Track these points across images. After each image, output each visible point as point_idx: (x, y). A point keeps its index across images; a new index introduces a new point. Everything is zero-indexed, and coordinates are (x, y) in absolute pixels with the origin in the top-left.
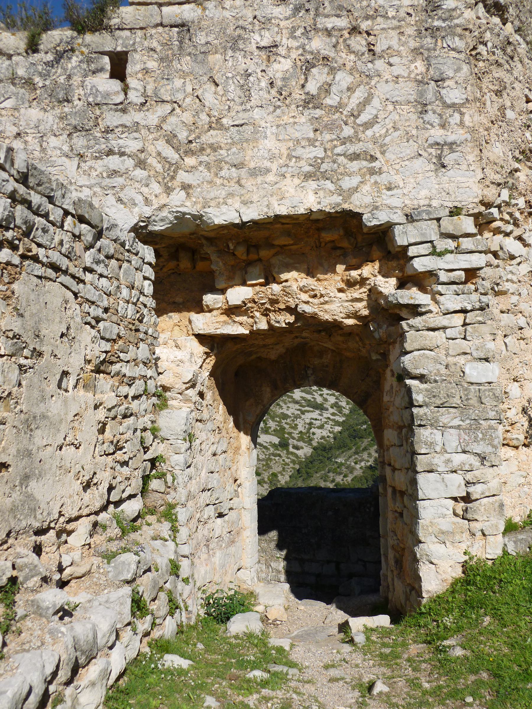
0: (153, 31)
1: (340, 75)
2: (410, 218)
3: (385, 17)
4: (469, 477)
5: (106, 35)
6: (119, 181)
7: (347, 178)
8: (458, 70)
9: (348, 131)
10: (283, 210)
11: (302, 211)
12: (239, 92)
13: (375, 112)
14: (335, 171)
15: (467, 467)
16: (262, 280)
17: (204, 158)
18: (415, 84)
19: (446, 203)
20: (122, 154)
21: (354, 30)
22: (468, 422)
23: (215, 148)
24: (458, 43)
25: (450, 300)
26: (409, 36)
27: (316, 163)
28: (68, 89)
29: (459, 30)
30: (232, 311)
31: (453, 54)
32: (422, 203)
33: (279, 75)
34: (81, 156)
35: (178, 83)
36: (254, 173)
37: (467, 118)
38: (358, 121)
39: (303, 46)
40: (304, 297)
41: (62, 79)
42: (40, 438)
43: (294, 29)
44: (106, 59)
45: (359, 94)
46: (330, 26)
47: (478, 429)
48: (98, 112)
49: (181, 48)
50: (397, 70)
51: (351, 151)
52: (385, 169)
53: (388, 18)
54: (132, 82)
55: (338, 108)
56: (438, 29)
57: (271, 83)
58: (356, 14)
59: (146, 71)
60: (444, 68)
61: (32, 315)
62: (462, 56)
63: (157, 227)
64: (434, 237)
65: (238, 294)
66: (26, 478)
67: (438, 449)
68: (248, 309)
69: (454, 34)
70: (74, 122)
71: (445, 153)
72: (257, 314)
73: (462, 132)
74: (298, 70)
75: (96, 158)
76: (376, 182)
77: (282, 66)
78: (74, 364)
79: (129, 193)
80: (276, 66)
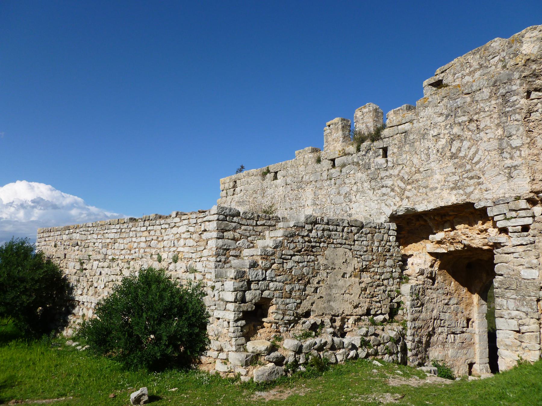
0: (396, 136)
1: (465, 142)
2: (495, 204)
3: (484, 112)
4: (520, 321)
5: (381, 141)
6: (386, 197)
7: (468, 188)
9: (468, 167)
10: (443, 204)
11: (450, 204)
12: (426, 157)
13: (480, 157)
14: (463, 185)
15: (519, 317)
16: (450, 229)
17: (414, 185)
19: (512, 195)
20: (387, 187)
21: (471, 121)
22: (520, 296)
23: (417, 181)
24: (518, 117)
25: (515, 240)
26: (495, 118)
27: (455, 183)
28: (369, 164)
29: (518, 110)
30: (440, 242)
32: (501, 196)
33: (441, 147)
34: (374, 189)
35: (404, 156)
36: (432, 189)
37: (523, 153)
38: (473, 162)
39: (449, 133)
40: (464, 237)
41: (367, 161)
42: (334, 291)
43: (446, 125)
44: (381, 150)
45: (473, 150)
47: (524, 300)
48: (379, 172)
49: (405, 142)
50: (489, 136)
51: (470, 176)
52: (484, 182)
54: (389, 158)
55: (464, 157)
56: (508, 112)
58: (471, 113)
59: (394, 153)
61: (331, 259)
62: (520, 123)
63: (400, 213)
65: (440, 235)
66: (329, 301)
67: (505, 308)
68: (444, 242)
69: (515, 113)
70: (371, 177)
71: (512, 171)
72: (448, 244)
73: (520, 160)
74: (448, 143)
75: (379, 189)
76: (481, 188)
78: (350, 269)
79: (389, 202)
80: (439, 143)
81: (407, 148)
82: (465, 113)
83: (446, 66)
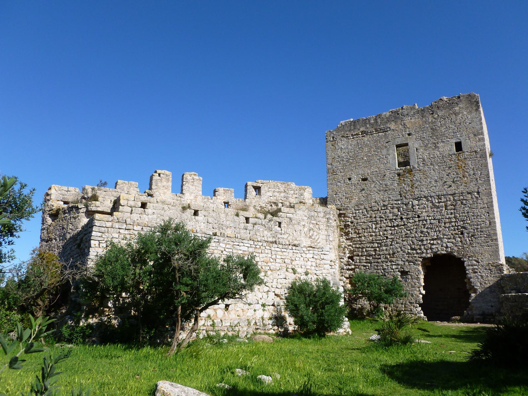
81: (291, 226)
82: (315, 220)
83: (265, 182)
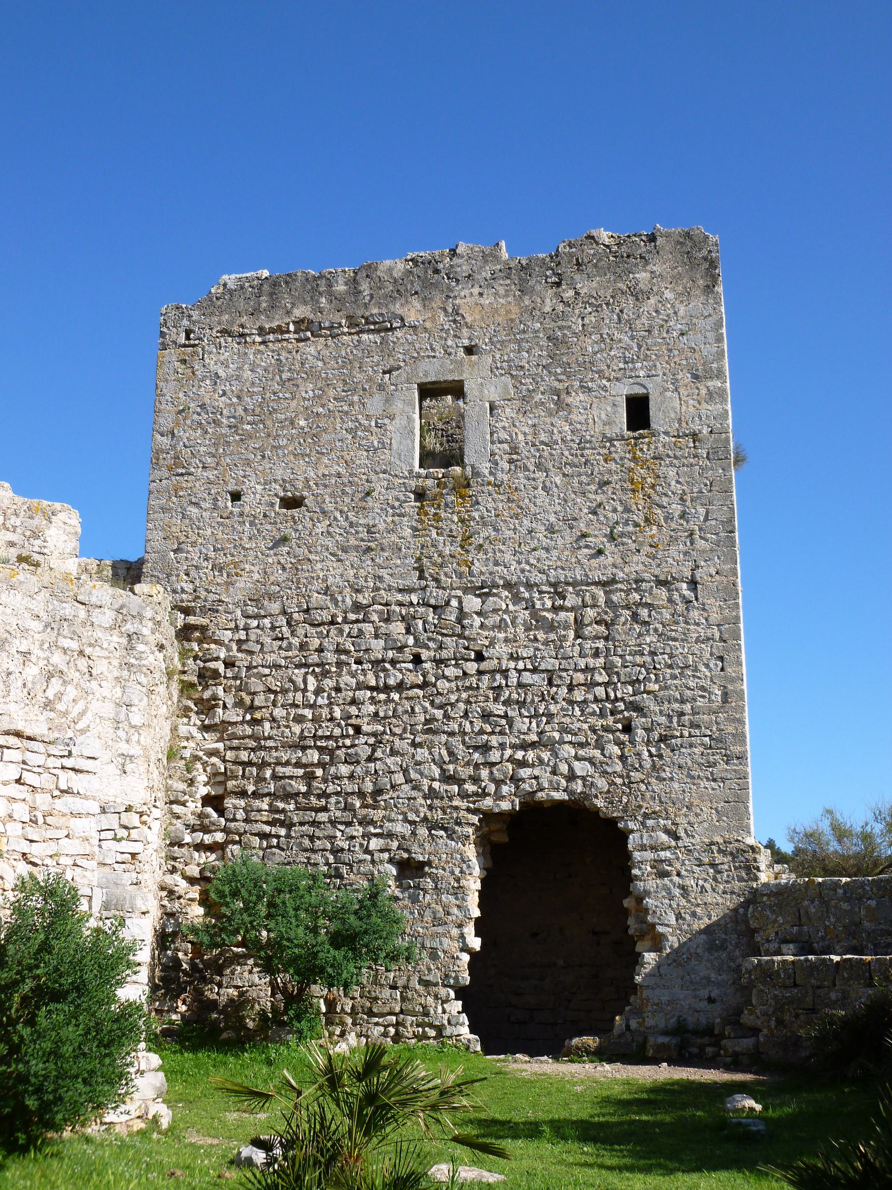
1: (70, 688)
8: (141, 700)
18: (114, 705)
24: (143, 680)
31: (139, 687)
33: (30, 679)
45: (80, 706)
46: (66, 646)
53: (102, 648)
55: (65, 714)
57: (24, 684)
60: (133, 697)
62: (144, 690)
64: (116, 826)
69: (141, 672)
73: (138, 748)
77: (32, 671)
